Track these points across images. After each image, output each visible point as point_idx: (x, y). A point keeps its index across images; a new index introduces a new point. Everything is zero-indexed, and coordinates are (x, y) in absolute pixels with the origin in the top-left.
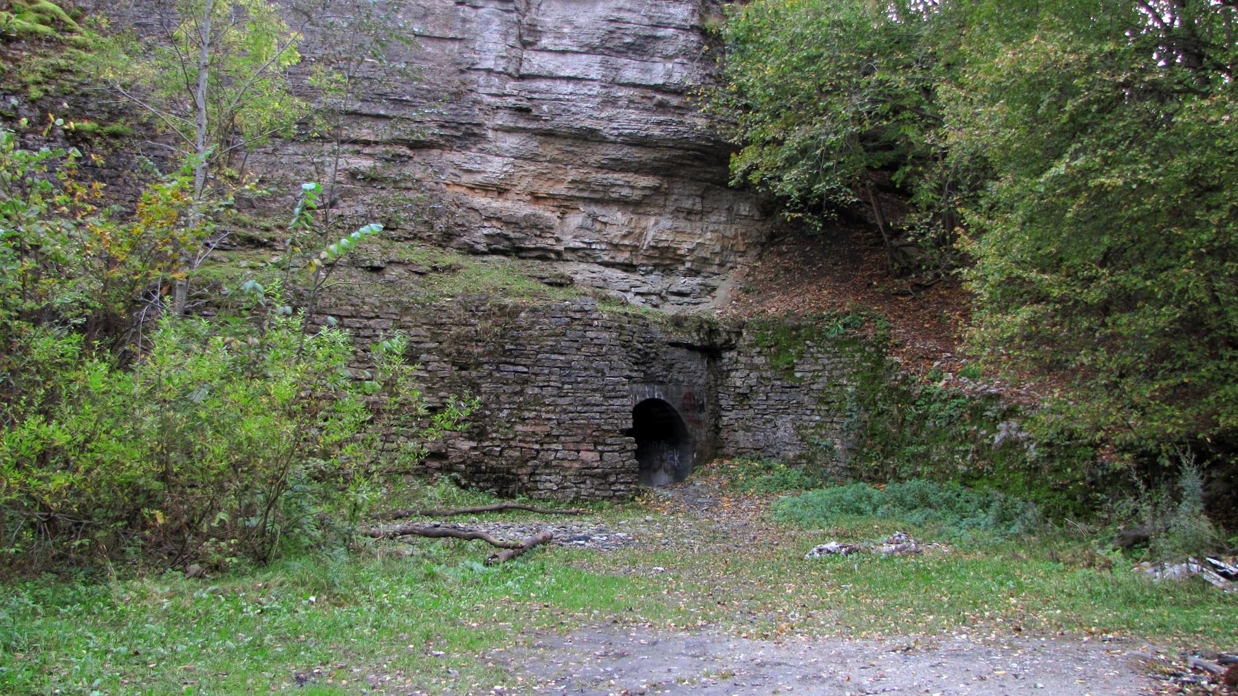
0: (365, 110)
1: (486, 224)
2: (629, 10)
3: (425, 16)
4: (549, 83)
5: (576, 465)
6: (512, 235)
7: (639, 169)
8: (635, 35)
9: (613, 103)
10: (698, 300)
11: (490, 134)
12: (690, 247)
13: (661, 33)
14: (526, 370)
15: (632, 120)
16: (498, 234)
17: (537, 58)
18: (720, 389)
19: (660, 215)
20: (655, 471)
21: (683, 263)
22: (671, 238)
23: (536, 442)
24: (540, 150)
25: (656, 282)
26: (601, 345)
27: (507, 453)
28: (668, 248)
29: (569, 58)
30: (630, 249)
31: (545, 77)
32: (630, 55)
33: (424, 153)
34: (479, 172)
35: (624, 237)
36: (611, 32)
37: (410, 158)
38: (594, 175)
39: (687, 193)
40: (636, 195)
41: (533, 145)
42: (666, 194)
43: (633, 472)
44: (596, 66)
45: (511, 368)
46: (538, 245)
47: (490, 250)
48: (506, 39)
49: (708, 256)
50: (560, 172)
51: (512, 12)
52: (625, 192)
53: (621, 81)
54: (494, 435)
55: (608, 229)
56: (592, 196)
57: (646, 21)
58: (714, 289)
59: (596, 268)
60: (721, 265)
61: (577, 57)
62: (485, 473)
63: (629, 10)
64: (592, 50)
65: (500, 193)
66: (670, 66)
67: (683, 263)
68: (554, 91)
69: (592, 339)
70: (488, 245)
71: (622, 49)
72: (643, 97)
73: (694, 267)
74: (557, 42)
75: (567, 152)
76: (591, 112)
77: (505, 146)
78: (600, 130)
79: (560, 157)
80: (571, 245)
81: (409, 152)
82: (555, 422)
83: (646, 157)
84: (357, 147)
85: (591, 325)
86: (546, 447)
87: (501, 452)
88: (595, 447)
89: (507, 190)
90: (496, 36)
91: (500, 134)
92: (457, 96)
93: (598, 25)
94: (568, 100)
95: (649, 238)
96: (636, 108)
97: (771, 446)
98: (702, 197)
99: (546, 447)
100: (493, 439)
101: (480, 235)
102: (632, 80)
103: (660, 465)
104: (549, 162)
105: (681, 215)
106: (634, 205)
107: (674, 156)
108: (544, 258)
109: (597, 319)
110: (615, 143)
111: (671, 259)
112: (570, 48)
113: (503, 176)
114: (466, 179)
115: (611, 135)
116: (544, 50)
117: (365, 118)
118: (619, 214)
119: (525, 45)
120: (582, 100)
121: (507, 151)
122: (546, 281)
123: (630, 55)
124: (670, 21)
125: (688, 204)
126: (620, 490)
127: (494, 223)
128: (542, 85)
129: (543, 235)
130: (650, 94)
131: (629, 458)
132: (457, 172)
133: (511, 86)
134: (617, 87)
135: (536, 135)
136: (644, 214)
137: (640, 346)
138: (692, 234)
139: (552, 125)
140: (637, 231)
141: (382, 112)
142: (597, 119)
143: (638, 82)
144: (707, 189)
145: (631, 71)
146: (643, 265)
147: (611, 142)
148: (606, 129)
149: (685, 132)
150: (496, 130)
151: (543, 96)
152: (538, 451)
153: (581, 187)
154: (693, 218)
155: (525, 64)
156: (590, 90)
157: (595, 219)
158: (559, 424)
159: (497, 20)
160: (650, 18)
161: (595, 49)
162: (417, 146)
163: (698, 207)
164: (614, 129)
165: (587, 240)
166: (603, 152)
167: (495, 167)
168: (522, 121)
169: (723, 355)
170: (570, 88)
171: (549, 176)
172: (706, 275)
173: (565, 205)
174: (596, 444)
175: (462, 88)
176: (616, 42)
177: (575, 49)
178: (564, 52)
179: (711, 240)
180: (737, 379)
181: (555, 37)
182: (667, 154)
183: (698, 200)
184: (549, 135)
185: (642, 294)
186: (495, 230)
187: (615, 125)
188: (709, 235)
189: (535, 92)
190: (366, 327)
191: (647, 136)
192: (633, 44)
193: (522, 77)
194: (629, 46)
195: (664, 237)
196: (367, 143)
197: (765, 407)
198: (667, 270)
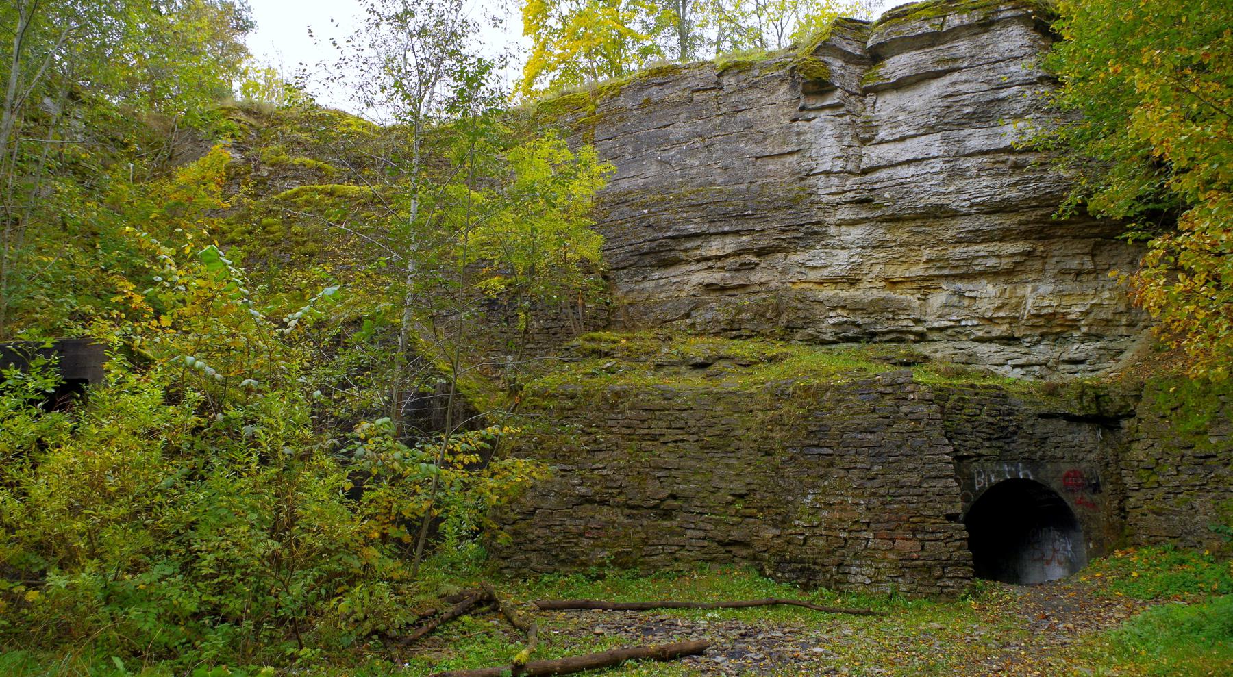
0: (712, 230)
1: (831, 314)
2: (966, 82)
3: (765, 139)
4: (891, 170)
5: (892, 556)
6: (860, 321)
7: (1004, 237)
8: (975, 103)
9: (961, 175)
10: (1097, 366)
11: (833, 230)
12: (1083, 310)
13: (1004, 93)
14: (830, 451)
15: (982, 188)
16: (846, 322)
17: (877, 151)
18: (1122, 464)
19: (1040, 280)
20: (1048, 563)
21: (1079, 328)
22: (1055, 303)
23: (844, 530)
24: (888, 236)
25: (1044, 351)
26: (918, 420)
27: (813, 541)
28: (1054, 314)
29: (908, 142)
30: (1008, 320)
31: (885, 167)
32: (974, 124)
33: (769, 258)
34: (825, 267)
35: (999, 308)
36: (948, 107)
37: (757, 264)
38: (951, 250)
39: (1070, 252)
40: (1006, 263)
41: (879, 232)
42: (1044, 258)
43: (965, 565)
44: (937, 144)
45: (816, 451)
46: (891, 328)
47: (840, 338)
48: (841, 141)
49: (1110, 317)
50: (913, 254)
51: (844, 115)
52: (991, 262)
53: (967, 152)
54: (797, 522)
55: (979, 304)
56: (953, 272)
57: (985, 86)
58: (1120, 352)
59: (968, 345)
60: (1131, 325)
61: (916, 140)
62: (790, 562)
63: (966, 82)
64: (930, 129)
65: (852, 284)
66: (1021, 124)
67: (1079, 328)
68: (895, 177)
69: (906, 414)
70: (836, 334)
71: (964, 121)
72: (994, 163)
73: (1093, 332)
74: (894, 131)
75: (918, 233)
76: (936, 189)
77: (850, 238)
78: (947, 205)
79: (911, 239)
80: (936, 325)
81: (754, 259)
82: (864, 507)
83: (1008, 222)
84: (710, 263)
85: (906, 399)
86: (854, 535)
87: (805, 540)
88: (914, 535)
89: (858, 280)
90: (832, 140)
91: (844, 228)
92: (796, 201)
93: (933, 104)
94: (910, 183)
95: (1029, 307)
96: (987, 176)
97: (1190, 533)
98: (1093, 256)
99: (854, 535)
100: (796, 526)
101: (828, 324)
102: (979, 148)
103: (1053, 556)
104: (900, 246)
105: (1068, 277)
106: (1008, 274)
107: (1042, 215)
108: (900, 341)
109: (913, 392)
110: (969, 214)
111: (1061, 325)
112: (907, 133)
113: (850, 267)
114: (812, 275)
115: (963, 207)
116: (882, 142)
117: (713, 237)
118: (990, 287)
119: (864, 142)
120: (925, 179)
121: (852, 243)
122: (893, 361)
123: (974, 124)
124: (1013, 79)
125: (1074, 264)
126: (948, 586)
127: (839, 311)
128: (883, 174)
129: (897, 317)
130: (1003, 157)
131: (959, 548)
132: (803, 270)
133: (852, 182)
134: (963, 159)
135: (881, 222)
136: (1020, 282)
137: (991, 420)
138: (1083, 296)
139: (894, 210)
140: (1013, 301)
141: (726, 229)
142: (945, 194)
143: (985, 148)
144: (1097, 246)
145: (977, 139)
146: (1028, 336)
147: (965, 214)
148: (956, 203)
149: (1046, 187)
150: (840, 225)
151: (884, 184)
152: (846, 540)
153: (939, 265)
154: (1084, 278)
155: (865, 160)
156: (932, 168)
157: (962, 296)
158: (868, 509)
159: (829, 125)
160: (989, 82)
161: (933, 127)
162: (761, 253)
163: (1089, 265)
164: (965, 200)
165: (954, 318)
166: (957, 226)
167: (841, 261)
168: (863, 212)
169: (1122, 425)
170: (912, 170)
171: (901, 259)
172: (1112, 338)
173: (925, 286)
174: (914, 531)
175: (802, 194)
176: (956, 115)
177: (913, 133)
178: (903, 139)
179: (1109, 299)
180: (1138, 451)
181: (892, 127)
182: (1033, 215)
183: (1087, 258)
184: (895, 220)
185: (1022, 366)
186: (841, 318)
187: (965, 196)
188: (1106, 294)
189: (876, 182)
190: (677, 418)
191: (1003, 200)
192: (974, 113)
193: (865, 172)
194: (970, 116)
195: (1046, 303)
196: (718, 258)
197: (1177, 483)
198: (1059, 338)
